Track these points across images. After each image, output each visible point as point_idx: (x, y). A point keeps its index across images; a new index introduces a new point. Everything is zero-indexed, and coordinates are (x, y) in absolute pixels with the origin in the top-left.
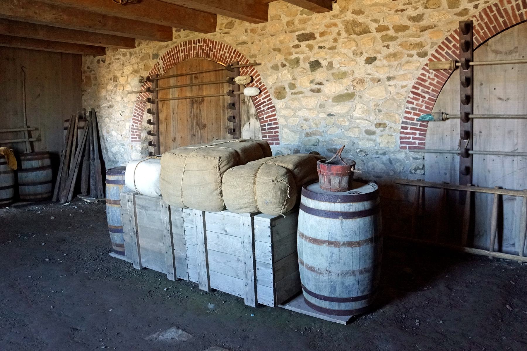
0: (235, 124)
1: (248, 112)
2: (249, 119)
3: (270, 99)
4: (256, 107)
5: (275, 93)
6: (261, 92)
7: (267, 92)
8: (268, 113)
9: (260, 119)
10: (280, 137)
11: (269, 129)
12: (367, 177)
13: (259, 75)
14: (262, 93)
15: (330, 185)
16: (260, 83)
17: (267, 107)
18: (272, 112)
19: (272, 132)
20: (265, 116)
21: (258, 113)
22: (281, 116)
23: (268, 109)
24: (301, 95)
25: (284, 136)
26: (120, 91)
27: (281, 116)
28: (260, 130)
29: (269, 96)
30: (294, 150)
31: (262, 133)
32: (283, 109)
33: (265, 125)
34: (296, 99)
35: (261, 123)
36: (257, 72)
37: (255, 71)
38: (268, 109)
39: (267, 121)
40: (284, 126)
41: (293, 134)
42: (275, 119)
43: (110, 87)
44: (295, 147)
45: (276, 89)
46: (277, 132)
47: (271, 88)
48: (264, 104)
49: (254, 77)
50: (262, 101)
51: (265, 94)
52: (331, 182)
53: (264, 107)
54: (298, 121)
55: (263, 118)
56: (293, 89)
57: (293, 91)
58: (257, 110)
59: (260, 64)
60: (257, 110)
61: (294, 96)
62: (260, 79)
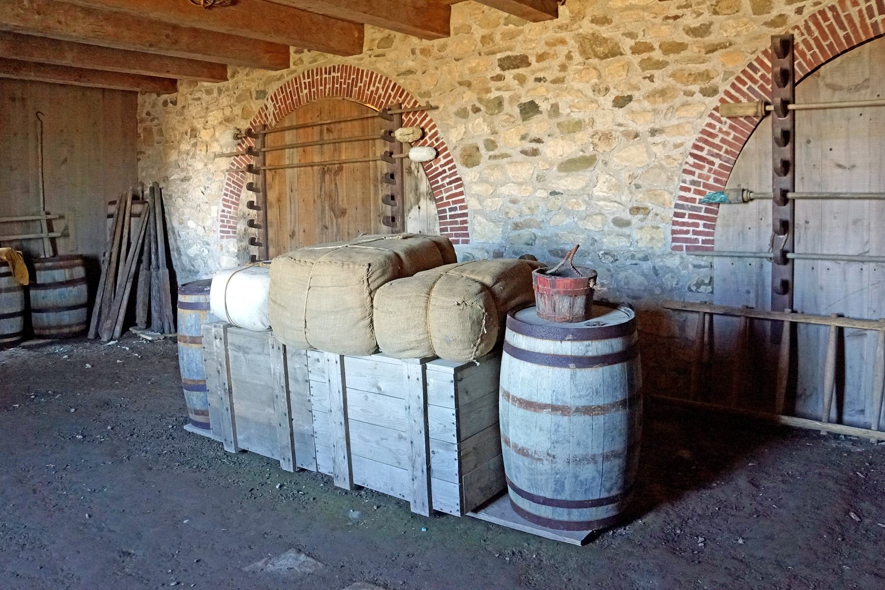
2: (418, 200)
3: (454, 167)
4: (430, 179)
6: (438, 154)
7: (448, 155)
8: (450, 189)
9: (436, 201)
10: (469, 231)
11: (451, 217)
14: (441, 157)
16: (437, 140)
17: (448, 180)
18: (456, 188)
19: (456, 223)
20: (445, 195)
21: (433, 189)
22: (473, 195)
23: (450, 183)
24: (505, 160)
25: (478, 228)
26: (201, 152)
27: (473, 195)
28: (437, 218)
29: (451, 161)
31: (441, 224)
32: (475, 183)
34: (497, 166)
35: (438, 206)
36: (431, 121)
37: (428, 119)
38: (450, 183)
39: (448, 203)
40: (476, 212)
41: (492, 225)
42: (463, 201)
44: (496, 248)
45: (464, 150)
46: (465, 222)
47: (455, 148)
48: (444, 175)
49: (427, 130)
50: (440, 170)
51: (444, 157)
53: (443, 179)
54: (500, 204)
55: (442, 199)
56: (493, 150)
57: (492, 153)
58: (431, 184)
59: (437, 108)
60: (431, 184)
61: (493, 162)
62: (436, 133)
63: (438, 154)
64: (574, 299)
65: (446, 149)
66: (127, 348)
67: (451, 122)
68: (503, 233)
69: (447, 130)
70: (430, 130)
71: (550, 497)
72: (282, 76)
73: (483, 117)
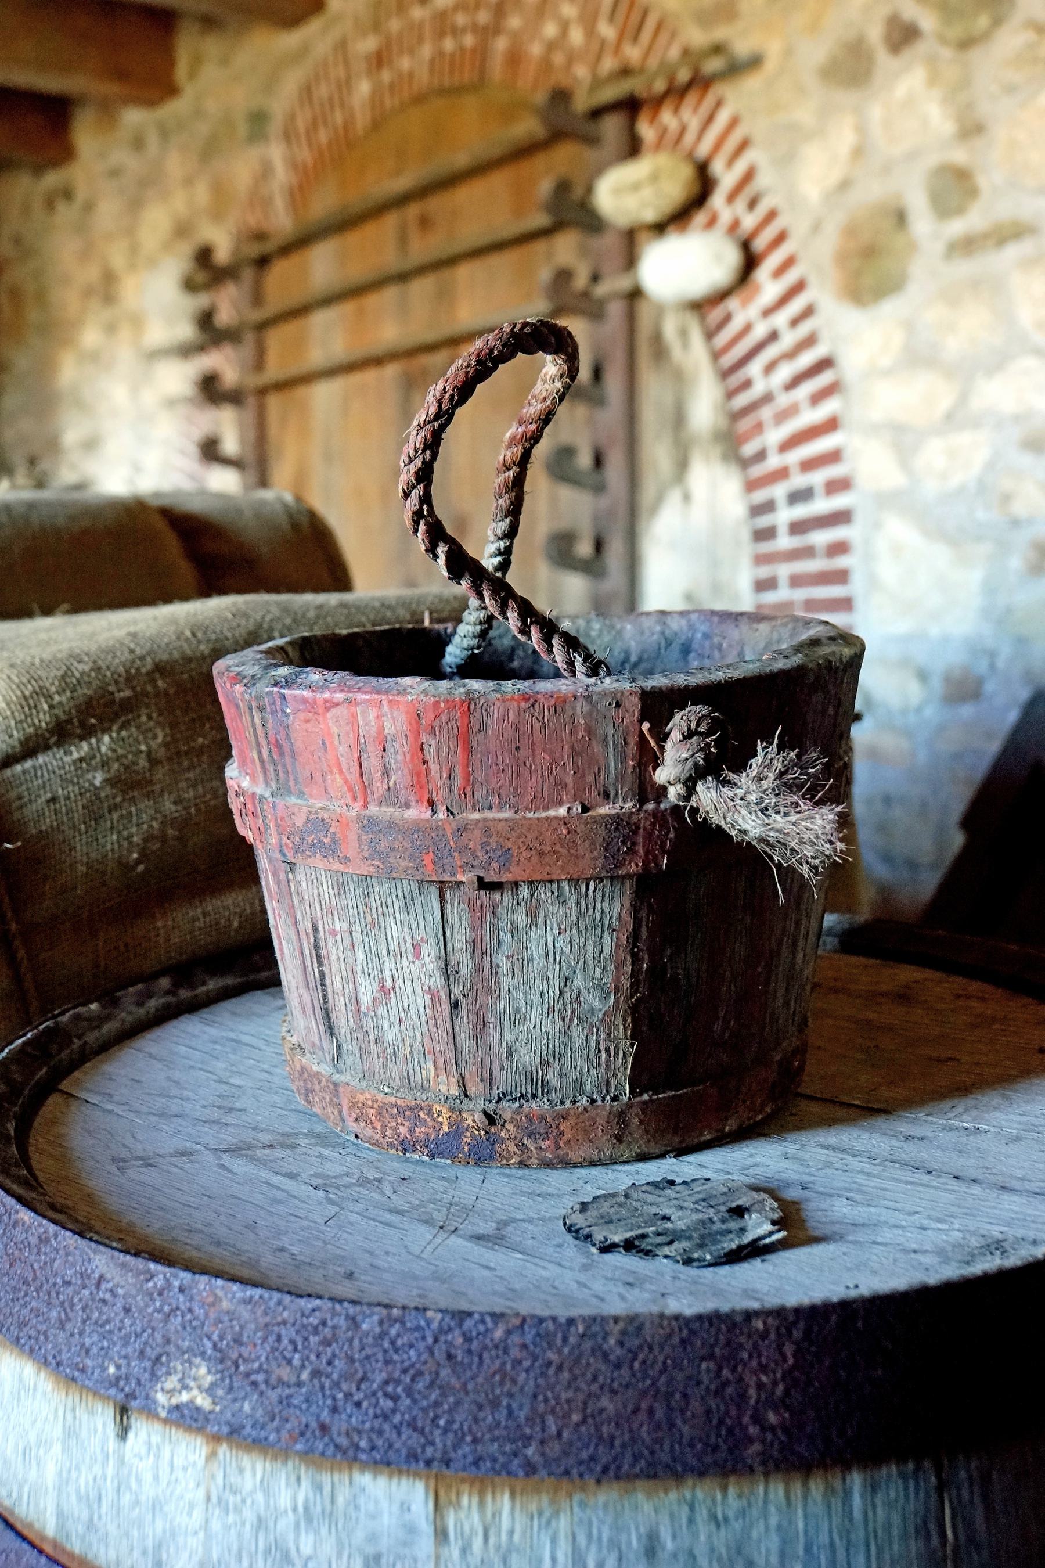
0: (604, 502)
1: (679, 419)
2: (682, 465)
3: (808, 312)
4: (725, 374)
5: (842, 258)
6: (750, 262)
7: (789, 263)
8: (791, 411)
9: (744, 464)
10: (856, 587)
11: (798, 528)
12: (924, 804)
13: (744, 145)
14: (763, 273)
15: (331, 1030)
16: (752, 204)
17: (785, 372)
18: (817, 398)
19: (808, 552)
20: (774, 436)
21: (736, 416)
22: (874, 429)
23: (794, 383)
24: (1012, 252)
25: (888, 571)
26: (125, 354)
27: (874, 429)
28: (746, 535)
29: (799, 287)
30: (948, 679)
31: (760, 560)
32: (887, 373)
33: (768, 507)
34: (975, 285)
35: (751, 486)
36: (734, 123)
37: (723, 117)
38: (794, 383)
39: (782, 474)
40: (886, 500)
41: (940, 555)
42: (833, 457)
43: (91, 337)
44: (954, 658)
45: (850, 231)
46: (839, 548)
47: (816, 228)
48: (772, 352)
49: (717, 167)
50: (760, 331)
51: (780, 271)
52: (336, 982)
53: (770, 368)
54: (980, 457)
55: (761, 456)
56: (960, 211)
57: (957, 227)
58: (730, 394)
59: (755, 62)
60: (730, 394)
61: (964, 268)
62: (749, 176)
63: (750, 262)
64: (479, 916)
65: (781, 238)
66: (759, 970)
67: (804, 114)
68: (990, 589)
69: (787, 159)
70: (731, 162)
71: (364, 1479)
72: (304, 51)
73: (932, 62)
